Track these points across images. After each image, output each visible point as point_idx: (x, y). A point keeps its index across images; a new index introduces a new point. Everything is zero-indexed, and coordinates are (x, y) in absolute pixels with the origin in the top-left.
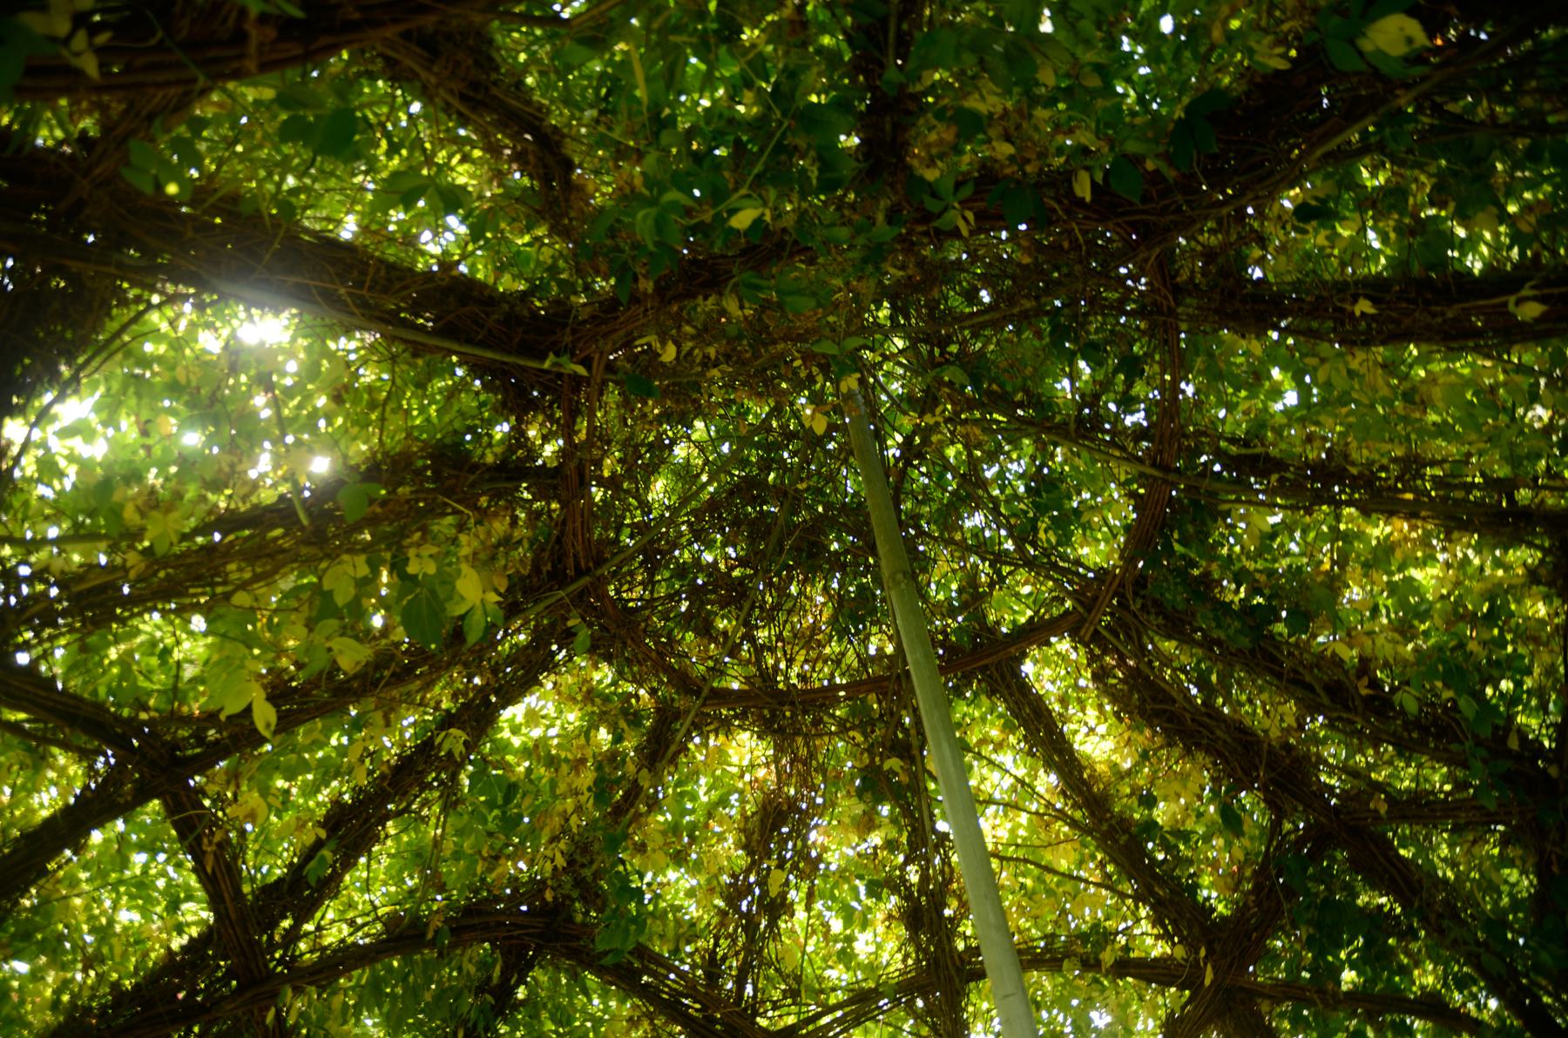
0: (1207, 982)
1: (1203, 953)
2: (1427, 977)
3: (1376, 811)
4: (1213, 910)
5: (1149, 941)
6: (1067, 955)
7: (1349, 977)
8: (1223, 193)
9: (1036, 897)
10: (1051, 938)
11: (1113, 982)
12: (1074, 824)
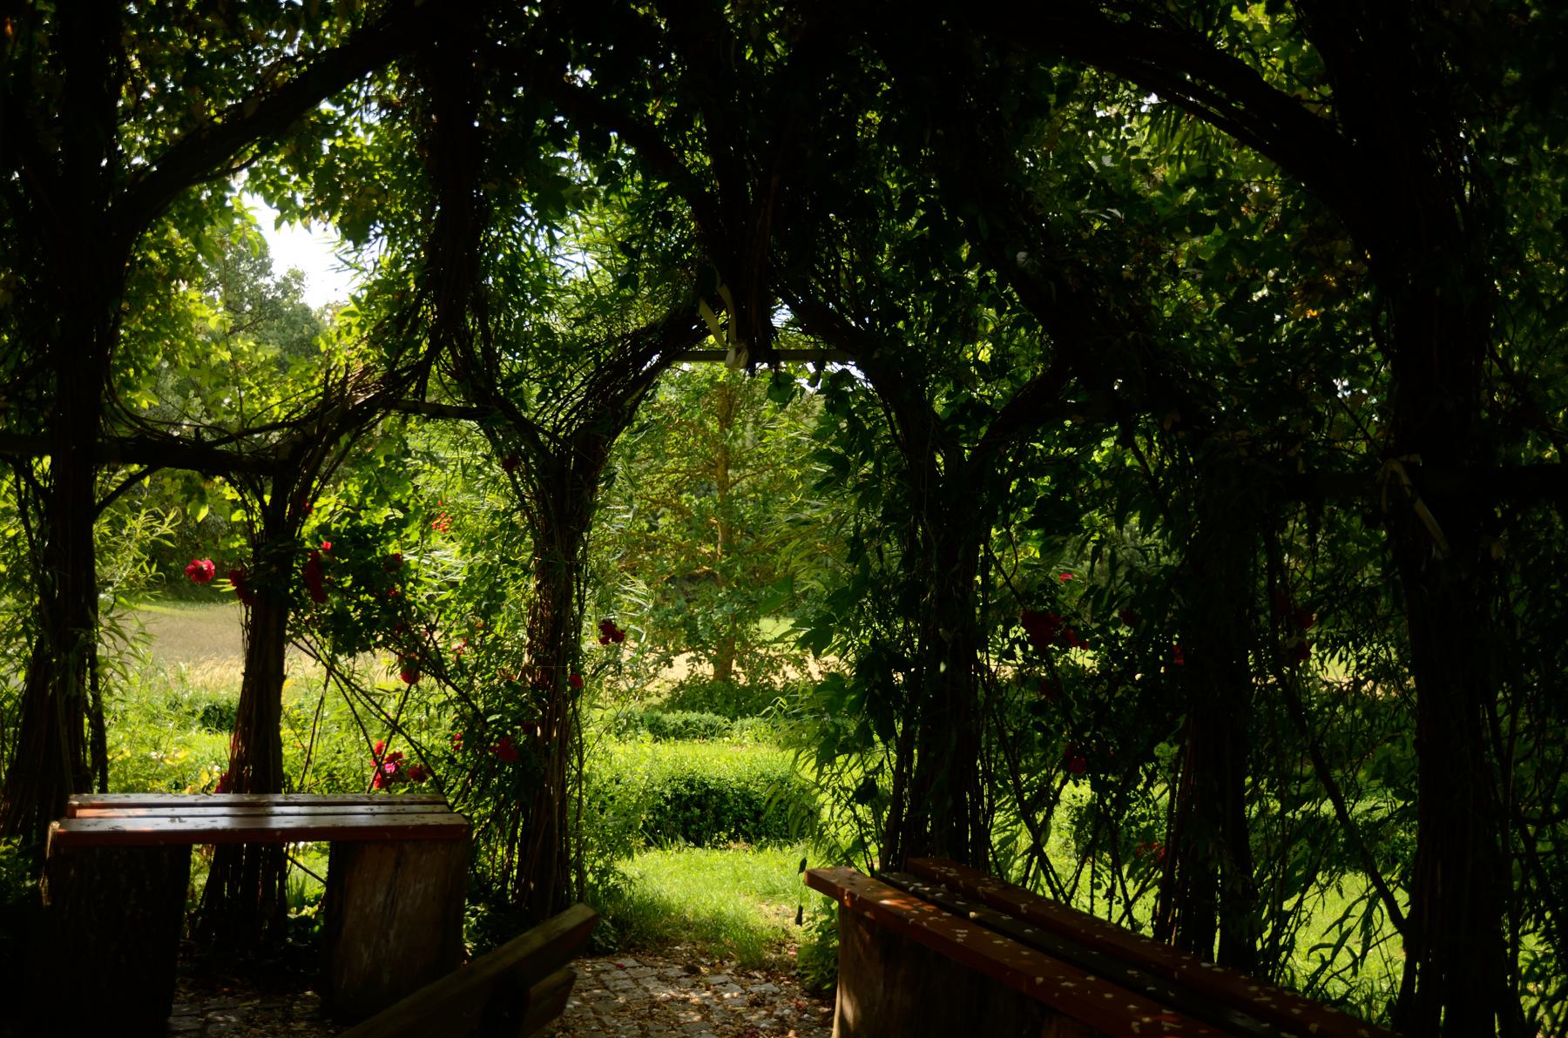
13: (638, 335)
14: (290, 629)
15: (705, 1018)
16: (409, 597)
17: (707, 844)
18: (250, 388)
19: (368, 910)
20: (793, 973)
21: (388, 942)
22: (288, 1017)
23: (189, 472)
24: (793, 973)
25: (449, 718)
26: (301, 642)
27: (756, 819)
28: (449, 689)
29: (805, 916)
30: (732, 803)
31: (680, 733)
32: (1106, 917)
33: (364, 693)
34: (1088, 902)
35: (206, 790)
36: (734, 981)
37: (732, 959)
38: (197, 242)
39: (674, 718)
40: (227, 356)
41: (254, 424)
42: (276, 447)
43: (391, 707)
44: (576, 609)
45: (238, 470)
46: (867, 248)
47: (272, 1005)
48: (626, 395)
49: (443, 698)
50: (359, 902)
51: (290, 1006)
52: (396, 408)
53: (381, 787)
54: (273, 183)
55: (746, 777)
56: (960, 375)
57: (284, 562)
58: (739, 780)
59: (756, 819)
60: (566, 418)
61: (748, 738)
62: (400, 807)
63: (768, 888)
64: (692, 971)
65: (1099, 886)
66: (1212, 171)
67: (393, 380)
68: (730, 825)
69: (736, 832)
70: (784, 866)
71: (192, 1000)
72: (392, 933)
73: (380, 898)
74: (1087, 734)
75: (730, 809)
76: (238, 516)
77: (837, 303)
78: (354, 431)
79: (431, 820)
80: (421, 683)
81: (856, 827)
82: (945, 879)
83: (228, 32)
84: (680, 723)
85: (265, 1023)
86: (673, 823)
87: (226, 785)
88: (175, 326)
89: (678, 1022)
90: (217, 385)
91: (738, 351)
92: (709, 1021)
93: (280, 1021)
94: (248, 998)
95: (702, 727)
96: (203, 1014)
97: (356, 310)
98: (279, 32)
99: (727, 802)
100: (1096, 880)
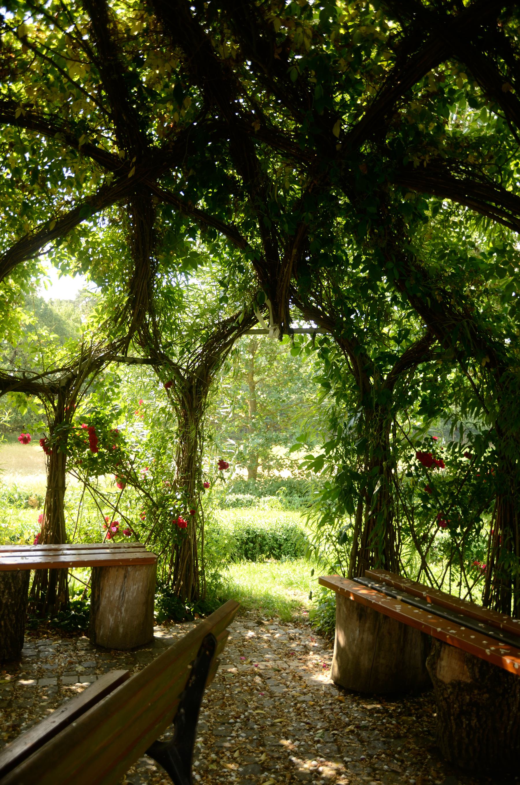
0: (130, 175)
1: (134, 160)
2: (237, 220)
3: (253, 128)
4: (152, 141)
5: (110, 143)
6: (60, 130)
7: (202, 203)
8: (425, 37)
9: (54, 89)
10: (54, 117)
11: (81, 156)
12: (90, 53)
13: (225, 324)
14: (68, 465)
15: (269, 646)
16: (123, 449)
17: (257, 560)
18: (47, 353)
19: (112, 598)
20: (307, 623)
21: (121, 613)
22: (76, 649)
23: (20, 393)
24: (307, 623)
25: (141, 504)
26: (72, 471)
27: (279, 548)
28: (141, 492)
29: (313, 595)
30: (268, 541)
31: (236, 504)
32: (457, 596)
33: (101, 494)
34: (448, 588)
35: (27, 542)
36: (280, 628)
37: (277, 617)
38: (22, 285)
39: (232, 498)
40: (36, 338)
41: (49, 370)
42: (59, 380)
43: (113, 500)
44: (199, 454)
45: (43, 391)
46: (336, 280)
47: (67, 643)
48: (221, 350)
49: (138, 496)
50: (107, 595)
51: (76, 643)
52: (114, 360)
53: (110, 538)
54: (58, 258)
55: (274, 528)
56: (382, 338)
57: (64, 434)
58: (271, 530)
59: (279, 548)
60: (192, 362)
61: (267, 506)
62: (125, 550)
63: (289, 582)
64: (260, 623)
65: (453, 580)
66: (505, 246)
67: (112, 347)
68: (267, 551)
69: (270, 554)
70: (294, 570)
71: (30, 641)
72: (123, 609)
73: (117, 593)
74: (447, 509)
75: (267, 544)
76: (42, 411)
77: (322, 306)
78: (95, 372)
79: (139, 555)
80: (126, 488)
81: (336, 553)
82: (385, 581)
83: (41, 191)
84: (234, 500)
85: (66, 651)
86: (240, 551)
87: (39, 540)
88: (11, 324)
89: (256, 648)
90: (33, 352)
91: (275, 330)
92: (271, 648)
93: (73, 650)
94: (55, 640)
95: (245, 502)
96: (37, 648)
97: (97, 315)
98: (63, 189)
99: (265, 540)
100: (452, 578)
